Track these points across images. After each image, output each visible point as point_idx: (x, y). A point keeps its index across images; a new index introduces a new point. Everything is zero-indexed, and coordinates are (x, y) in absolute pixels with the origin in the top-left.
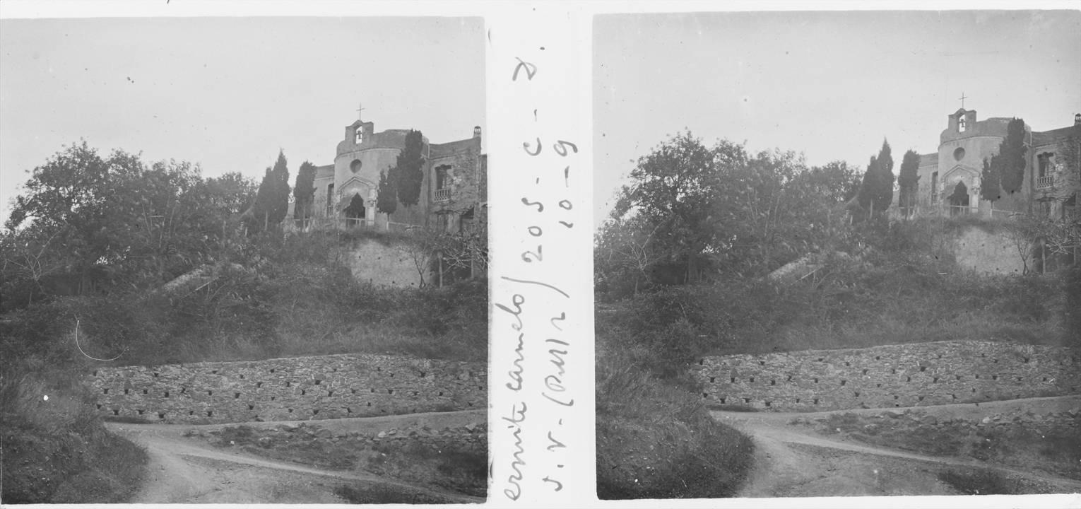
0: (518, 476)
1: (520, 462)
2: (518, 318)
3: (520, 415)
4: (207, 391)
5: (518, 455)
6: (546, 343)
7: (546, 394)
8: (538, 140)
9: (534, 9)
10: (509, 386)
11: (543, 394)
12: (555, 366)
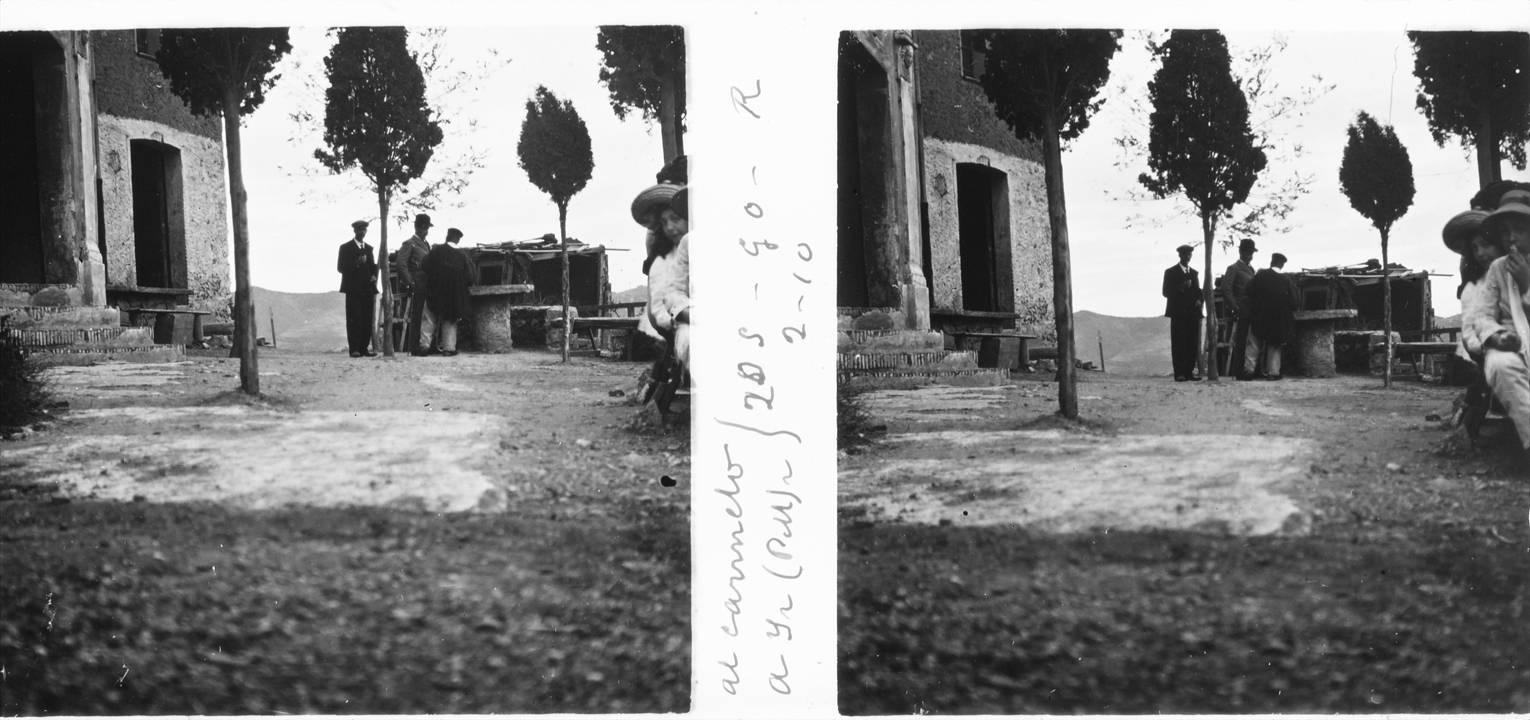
0: (739, 576)
1: (740, 543)
2: (735, 483)
3: (733, 468)
4: (523, 387)
5: (738, 558)
6: (715, 493)
7: (787, 635)
8: (720, 663)
9: (756, 13)
10: (769, 634)
11: (726, 446)
12: (780, 524)
